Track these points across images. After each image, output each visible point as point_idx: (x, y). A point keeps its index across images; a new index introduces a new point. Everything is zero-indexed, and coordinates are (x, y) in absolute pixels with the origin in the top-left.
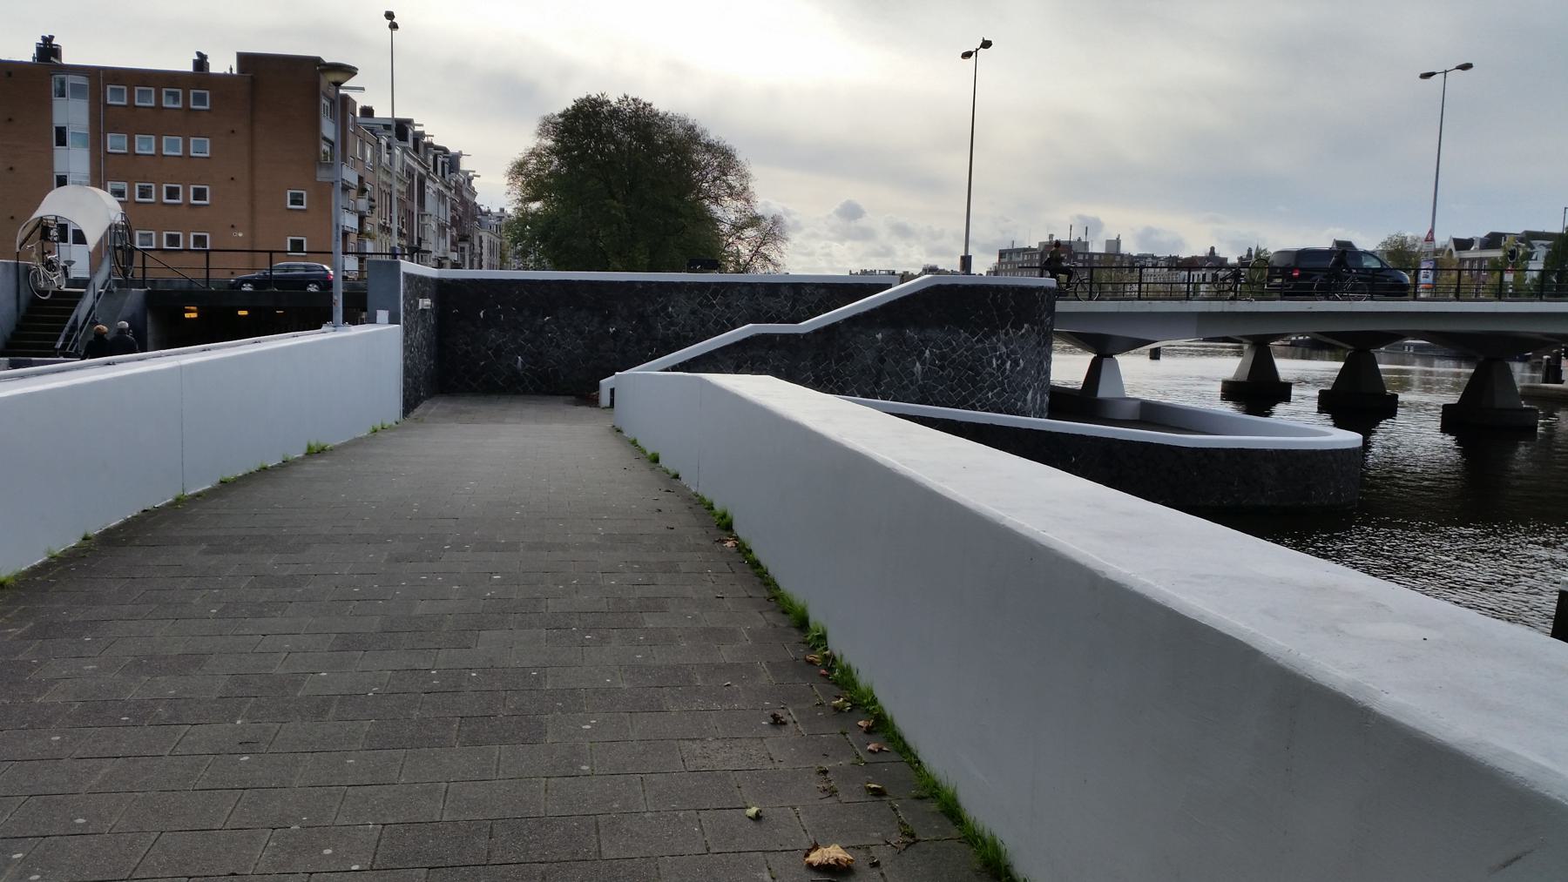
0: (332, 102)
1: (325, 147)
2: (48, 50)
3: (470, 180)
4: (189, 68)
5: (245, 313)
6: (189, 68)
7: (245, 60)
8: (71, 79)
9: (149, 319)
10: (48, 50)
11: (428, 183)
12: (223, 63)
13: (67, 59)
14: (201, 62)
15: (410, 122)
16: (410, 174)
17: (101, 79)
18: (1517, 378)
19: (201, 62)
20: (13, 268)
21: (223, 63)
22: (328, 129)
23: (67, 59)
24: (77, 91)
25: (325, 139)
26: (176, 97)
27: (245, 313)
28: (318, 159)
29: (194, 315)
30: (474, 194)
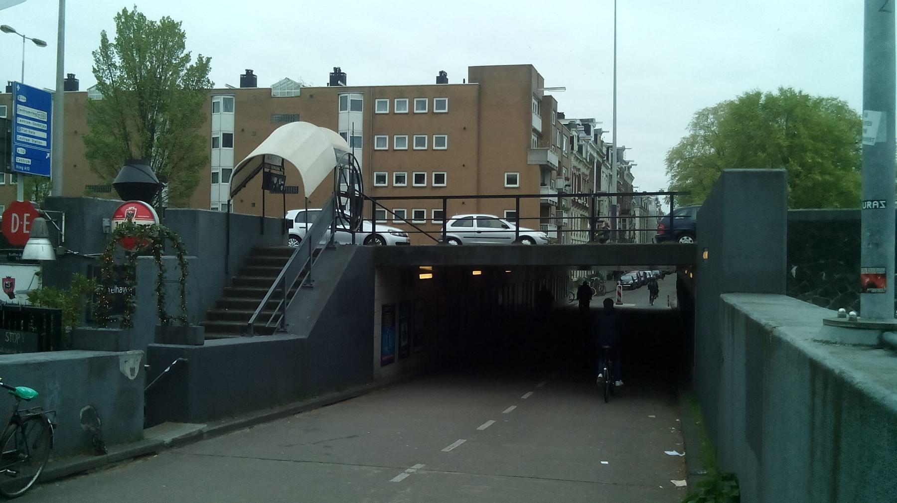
0: (540, 102)
1: (534, 138)
2: (338, 76)
3: (629, 168)
4: (434, 82)
5: (479, 273)
6: (434, 82)
7: (475, 72)
8: (351, 97)
9: (376, 277)
10: (338, 76)
11: (603, 169)
12: (458, 76)
13: (349, 83)
14: (442, 77)
15: (592, 120)
16: (592, 161)
17: (373, 93)
18: (666, 307)
19: (442, 77)
20: (477, 87)
21: (458, 76)
22: (537, 123)
23: (349, 83)
24: (356, 106)
25: (535, 130)
26: (422, 105)
27: (479, 273)
28: (529, 146)
29: (429, 276)
30: (632, 178)
